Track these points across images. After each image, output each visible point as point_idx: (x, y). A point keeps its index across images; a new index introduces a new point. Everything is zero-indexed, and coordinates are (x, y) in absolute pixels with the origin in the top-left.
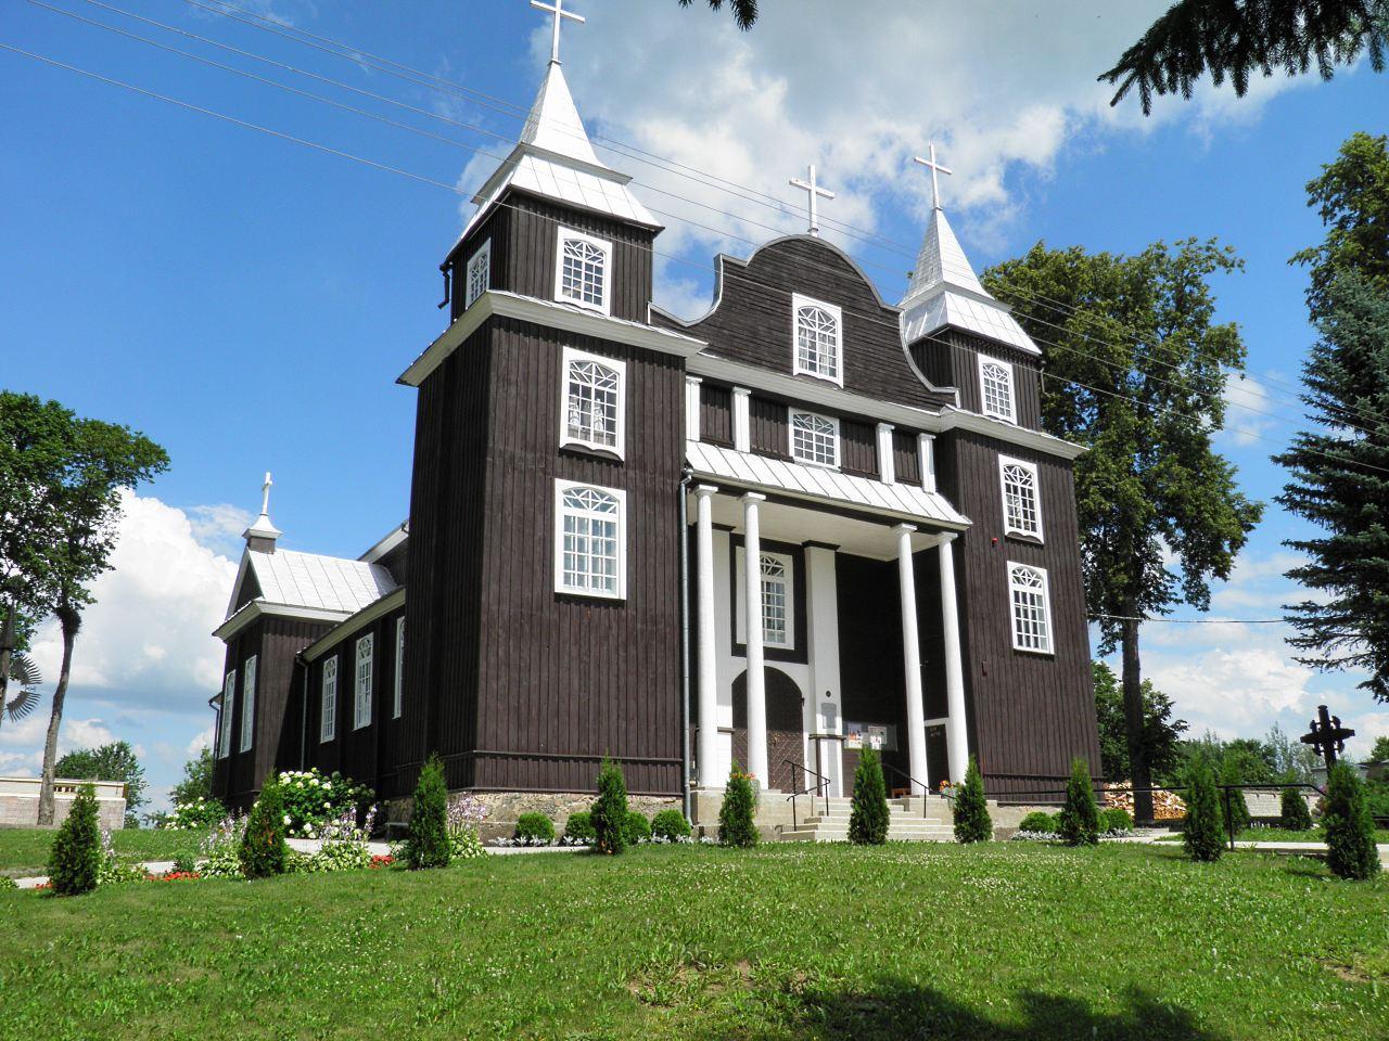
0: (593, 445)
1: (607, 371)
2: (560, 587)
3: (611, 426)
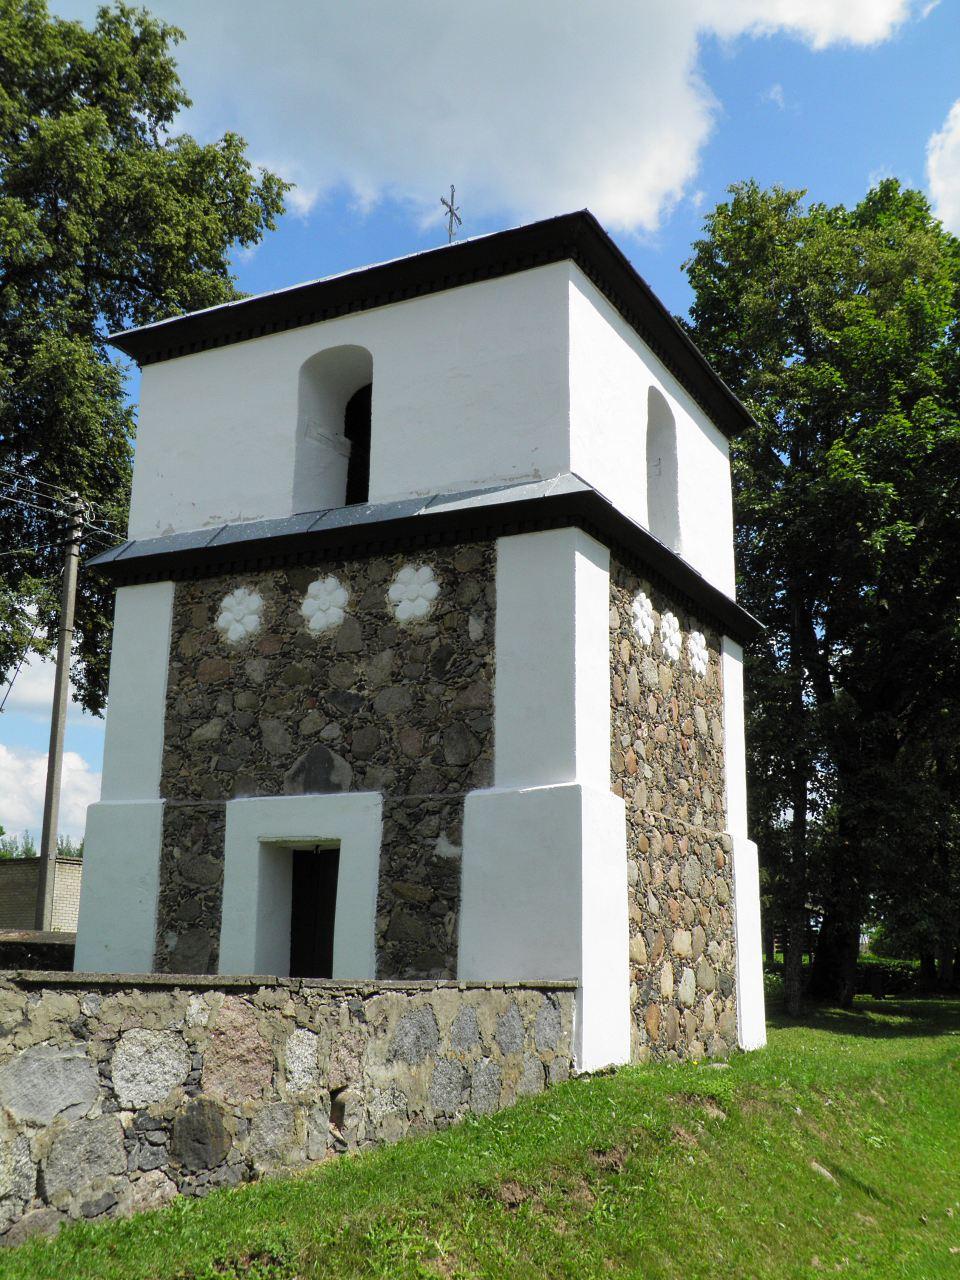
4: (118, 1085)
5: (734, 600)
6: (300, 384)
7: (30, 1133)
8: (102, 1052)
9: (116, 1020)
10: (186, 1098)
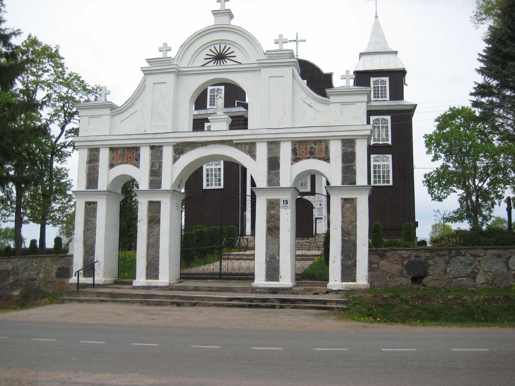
0: (381, 143)
1: (384, 120)
2: (205, 187)
3: (387, 135)
4: (510, 266)
7: (489, 273)
8: (506, 260)
9: (509, 254)
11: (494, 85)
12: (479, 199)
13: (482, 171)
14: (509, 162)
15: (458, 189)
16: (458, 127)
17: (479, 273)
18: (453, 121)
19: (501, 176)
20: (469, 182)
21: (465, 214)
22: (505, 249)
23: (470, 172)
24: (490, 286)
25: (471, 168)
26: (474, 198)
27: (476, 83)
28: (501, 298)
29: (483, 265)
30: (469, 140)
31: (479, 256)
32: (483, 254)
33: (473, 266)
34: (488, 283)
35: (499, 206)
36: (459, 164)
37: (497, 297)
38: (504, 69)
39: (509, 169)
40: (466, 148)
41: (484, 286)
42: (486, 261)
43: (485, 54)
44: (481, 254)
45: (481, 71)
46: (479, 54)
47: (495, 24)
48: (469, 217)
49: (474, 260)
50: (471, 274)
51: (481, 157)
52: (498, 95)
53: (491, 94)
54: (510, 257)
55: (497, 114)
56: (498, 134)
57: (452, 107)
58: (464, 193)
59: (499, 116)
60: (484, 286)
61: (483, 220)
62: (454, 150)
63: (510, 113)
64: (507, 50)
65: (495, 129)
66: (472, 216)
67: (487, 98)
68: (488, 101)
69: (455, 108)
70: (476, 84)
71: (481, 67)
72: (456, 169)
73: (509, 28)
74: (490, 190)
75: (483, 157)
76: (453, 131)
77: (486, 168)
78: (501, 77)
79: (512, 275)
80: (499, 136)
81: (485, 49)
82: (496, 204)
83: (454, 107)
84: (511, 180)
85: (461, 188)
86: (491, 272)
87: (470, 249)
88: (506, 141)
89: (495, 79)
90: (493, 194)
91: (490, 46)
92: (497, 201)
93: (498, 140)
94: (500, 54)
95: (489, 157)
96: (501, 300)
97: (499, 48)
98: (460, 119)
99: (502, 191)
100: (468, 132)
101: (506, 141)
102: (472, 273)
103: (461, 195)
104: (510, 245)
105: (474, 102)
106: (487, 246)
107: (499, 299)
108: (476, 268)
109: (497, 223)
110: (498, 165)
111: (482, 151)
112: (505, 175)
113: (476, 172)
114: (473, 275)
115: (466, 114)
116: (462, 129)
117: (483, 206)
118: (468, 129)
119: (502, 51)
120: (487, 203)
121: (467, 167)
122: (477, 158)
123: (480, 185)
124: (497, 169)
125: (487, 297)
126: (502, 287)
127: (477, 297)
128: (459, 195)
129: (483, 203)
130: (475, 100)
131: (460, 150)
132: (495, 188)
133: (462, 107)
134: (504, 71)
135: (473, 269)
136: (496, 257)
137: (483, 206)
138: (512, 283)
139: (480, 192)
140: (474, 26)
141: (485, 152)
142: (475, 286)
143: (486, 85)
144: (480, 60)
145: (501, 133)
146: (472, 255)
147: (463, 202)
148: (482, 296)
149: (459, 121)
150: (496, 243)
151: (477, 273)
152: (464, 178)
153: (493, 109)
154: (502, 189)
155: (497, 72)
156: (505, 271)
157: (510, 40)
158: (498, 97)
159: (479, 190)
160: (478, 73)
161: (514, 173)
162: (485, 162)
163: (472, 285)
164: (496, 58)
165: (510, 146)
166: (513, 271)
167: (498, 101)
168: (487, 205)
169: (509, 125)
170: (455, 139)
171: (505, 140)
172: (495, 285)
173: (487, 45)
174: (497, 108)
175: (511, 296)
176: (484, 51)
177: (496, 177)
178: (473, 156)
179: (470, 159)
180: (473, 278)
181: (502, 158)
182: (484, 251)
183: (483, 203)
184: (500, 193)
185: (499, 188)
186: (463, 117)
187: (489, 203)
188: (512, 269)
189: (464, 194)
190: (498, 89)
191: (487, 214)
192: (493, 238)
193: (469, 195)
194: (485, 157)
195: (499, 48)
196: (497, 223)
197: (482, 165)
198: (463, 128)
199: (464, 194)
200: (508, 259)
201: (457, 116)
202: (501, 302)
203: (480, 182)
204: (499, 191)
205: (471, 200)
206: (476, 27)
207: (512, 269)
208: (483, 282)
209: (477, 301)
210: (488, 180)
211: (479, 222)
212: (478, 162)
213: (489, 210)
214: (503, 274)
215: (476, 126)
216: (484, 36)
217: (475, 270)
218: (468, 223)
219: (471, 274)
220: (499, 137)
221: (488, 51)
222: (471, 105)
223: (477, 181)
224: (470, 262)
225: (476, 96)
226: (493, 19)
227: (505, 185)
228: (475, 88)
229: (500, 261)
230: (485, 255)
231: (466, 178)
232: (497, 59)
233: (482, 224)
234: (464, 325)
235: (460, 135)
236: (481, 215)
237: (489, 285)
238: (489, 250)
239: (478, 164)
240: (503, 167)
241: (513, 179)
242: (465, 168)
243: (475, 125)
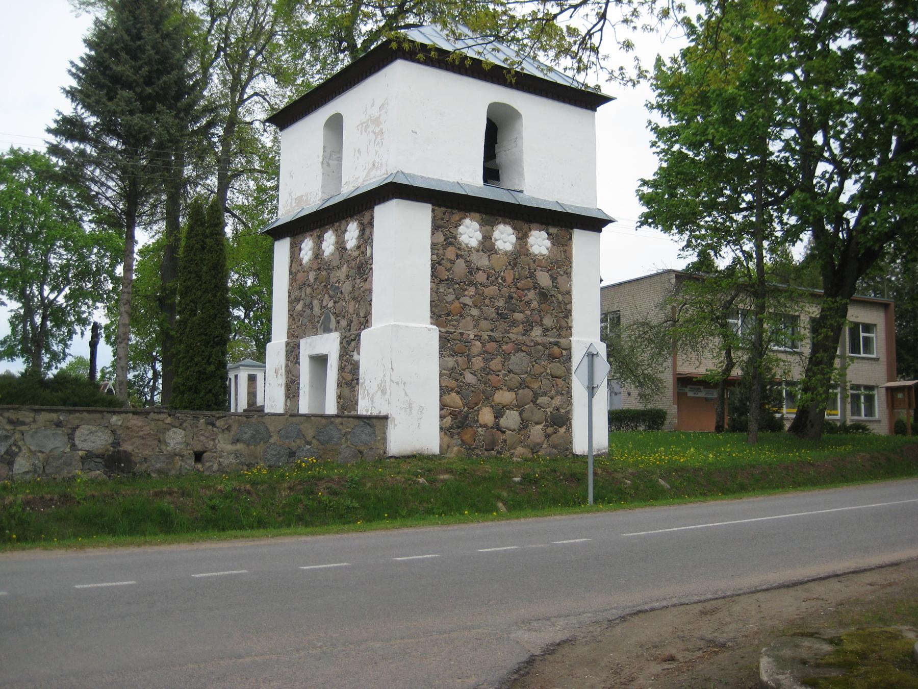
4: (77, 442)
5: (648, 210)
6: (325, 136)
7: (39, 454)
8: (70, 431)
9: (77, 422)
10: (112, 448)
11: (92, 124)
12: (48, 323)
13: (57, 272)
14: (106, 264)
15: (11, 299)
16: (23, 187)
17: (21, 454)
18: (14, 174)
19: (90, 285)
20: (32, 289)
21: (19, 347)
22: (70, 412)
23: (36, 272)
24: (38, 477)
25: (39, 264)
26: (38, 320)
27: (60, 113)
28: (56, 497)
29: (27, 438)
30: (41, 214)
31: (23, 423)
32: (31, 419)
33: (11, 441)
34: (35, 471)
35: (82, 337)
36: (16, 255)
37: (48, 496)
38: (111, 99)
39: (105, 275)
40: (33, 228)
41: (28, 477)
42: (35, 433)
43: (82, 65)
44: (27, 420)
45: (71, 93)
46: (72, 63)
47: (108, 18)
48: (25, 352)
49: (13, 430)
50: (5, 456)
51: (59, 247)
52: (95, 142)
53: (83, 138)
54: (78, 427)
55: (89, 175)
56: (93, 212)
57: (16, 148)
58: (21, 308)
59: (93, 180)
60: (28, 477)
61: (51, 359)
62: (11, 228)
63: (112, 179)
64: (119, 69)
65: (88, 199)
66: (31, 351)
67: (76, 144)
68: (76, 149)
69: (22, 151)
70: (59, 115)
71: (71, 87)
72: (11, 263)
73: (128, 31)
74: (69, 308)
75: (62, 247)
76: (13, 192)
77: (65, 268)
78: (104, 112)
79: (78, 458)
80: (94, 215)
81: (84, 56)
82: (76, 333)
83: (20, 149)
84: (106, 294)
85: (16, 299)
86: (42, 452)
87: (8, 410)
88: (105, 226)
89: (93, 113)
90: (74, 316)
91: (93, 53)
92: (78, 328)
93: (91, 221)
94: (108, 72)
95: (73, 250)
96: (54, 502)
97: (108, 62)
98: (28, 172)
99: (89, 313)
100: (40, 199)
101: (105, 226)
102: (7, 453)
103: (15, 311)
104: (88, 405)
105: (53, 145)
106: (49, 405)
107: (51, 500)
108: (15, 444)
109: (77, 368)
110: (86, 266)
111: (61, 236)
112: (97, 284)
113: (46, 273)
114: (9, 457)
115: (39, 166)
116: (30, 192)
117: (53, 336)
118: (41, 193)
119: (111, 69)
120: (60, 331)
121: (31, 262)
122: (51, 247)
123: (52, 297)
124: (84, 273)
125: (30, 496)
126: (59, 478)
127: (11, 498)
128: (11, 311)
129: (54, 329)
130: (55, 143)
131: (22, 228)
132: (77, 304)
133: (35, 152)
134: (110, 104)
135: (10, 446)
136: (54, 426)
137: (53, 336)
138: (77, 471)
139: (50, 310)
140: (72, 11)
141: (68, 239)
142: (11, 478)
143: (77, 120)
144: (73, 75)
145: (97, 211)
146: (11, 422)
147: (18, 325)
148: (20, 496)
149: (25, 175)
150: (64, 402)
151: (15, 455)
152: (24, 282)
153: (84, 166)
154: (89, 308)
155: (98, 102)
156: (68, 450)
157: (127, 53)
158: (96, 147)
159: (48, 307)
160: (65, 95)
161: (112, 283)
162: (65, 257)
163: (5, 476)
164: (101, 77)
165: (110, 236)
166: (81, 450)
167: (95, 154)
168: (61, 335)
169: (107, 198)
170: (15, 208)
171: (105, 224)
172: (47, 475)
173: (87, 50)
174: (91, 166)
175: (73, 495)
176: (82, 59)
177: (81, 287)
178: (44, 243)
179: (40, 249)
180: (8, 463)
181: (95, 254)
182: (32, 415)
183: (54, 329)
184: (84, 316)
185: (83, 306)
186: (34, 170)
187: (65, 329)
188: (80, 448)
189: (20, 310)
190: (98, 132)
191: (60, 350)
192: (60, 393)
193: (29, 312)
194: (66, 247)
195: (108, 62)
196: (77, 368)
197: (60, 262)
198: (31, 189)
199: (20, 310)
200: (74, 430)
201: (23, 166)
202: (55, 505)
203: (52, 291)
204: (84, 312)
205: (33, 324)
206: (75, 13)
207: (80, 447)
208: (27, 470)
209: (11, 505)
210: (67, 291)
211: (44, 363)
212: (52, 256)
213: (64, 343)
214: (63, 456)
215: (56, 192)
216: (88, 35)
217: (14, 448)
218: (24, 363)
219: (5, 456)
220: (94, 217)
221: (88, 59)
222: (46, 149)
223: (47, 289)
224: (5, 433)
225: (56, 136)
226: (107, 9)
227: (94, 301)
228: (56, 121)
229: (60, 432)
230: (34, 421)
231: (28, 281)
232: (103, 80)
233: (49, 367)
234: (409, 524)
235: (25, 203)
236: (48, 350)
237: (36, 476)
238: (43, 413)
239: (53, 260)
240: (95, 269)
241: (109, 293)
242: (26, 264)
243: (54, 188)
